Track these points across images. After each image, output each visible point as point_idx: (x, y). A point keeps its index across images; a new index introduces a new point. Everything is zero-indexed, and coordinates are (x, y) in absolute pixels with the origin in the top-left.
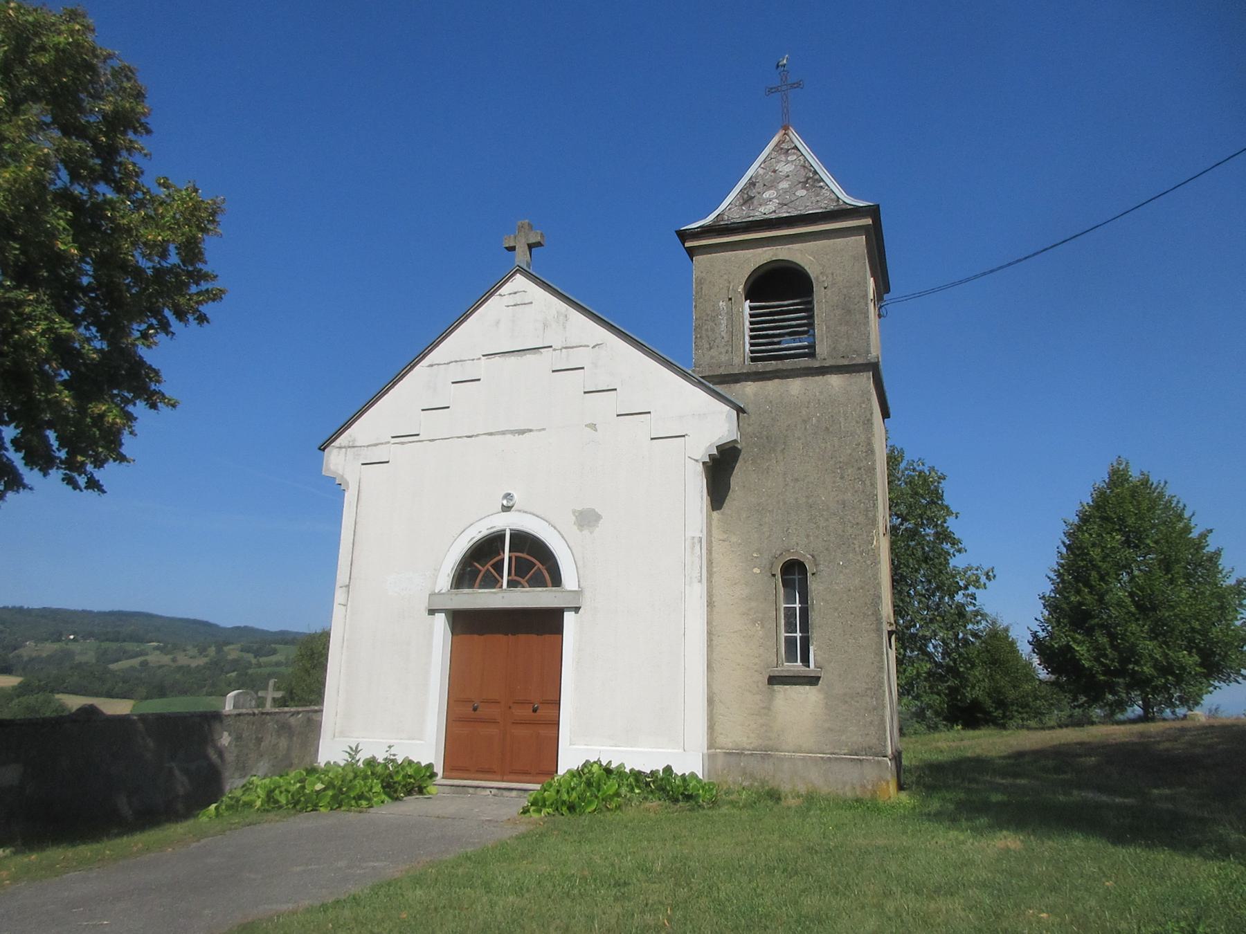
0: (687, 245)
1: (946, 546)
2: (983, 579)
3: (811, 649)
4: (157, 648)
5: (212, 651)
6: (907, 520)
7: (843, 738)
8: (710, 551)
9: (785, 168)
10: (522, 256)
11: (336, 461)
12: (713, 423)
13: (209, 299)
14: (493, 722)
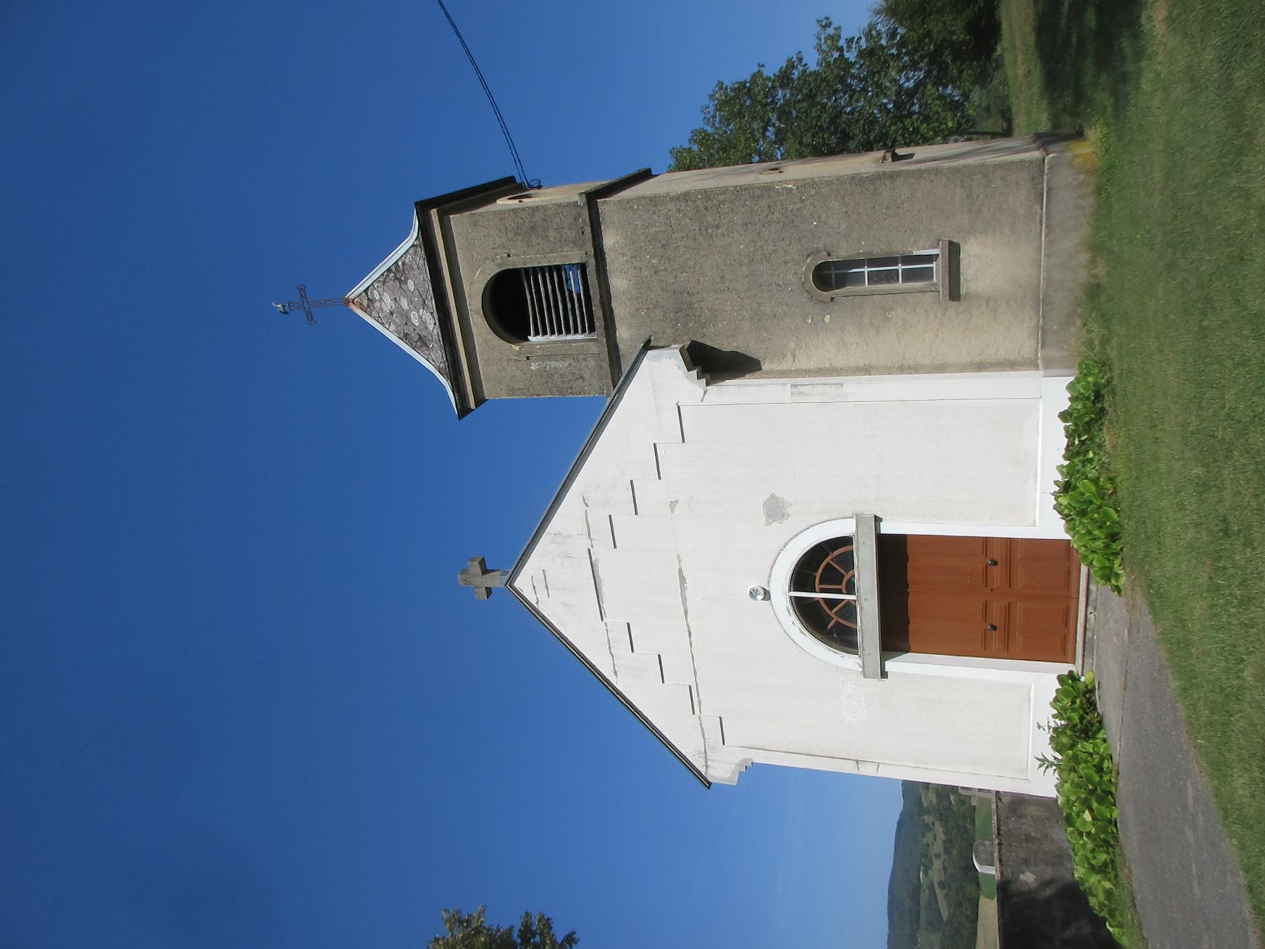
0: (473, 406)
1: (796, 74)
2: (830, 31)
3: (916, 253)
4: (926, 873)
5: (928, 819)
6: (769, 120)
7: (1022, 211)
8: (807, 373)
9: (388, 303)
10: (496, 580)
11: (721, 770)
12: (662, 377)
13: (549, 933)
14: (1008, 609)
